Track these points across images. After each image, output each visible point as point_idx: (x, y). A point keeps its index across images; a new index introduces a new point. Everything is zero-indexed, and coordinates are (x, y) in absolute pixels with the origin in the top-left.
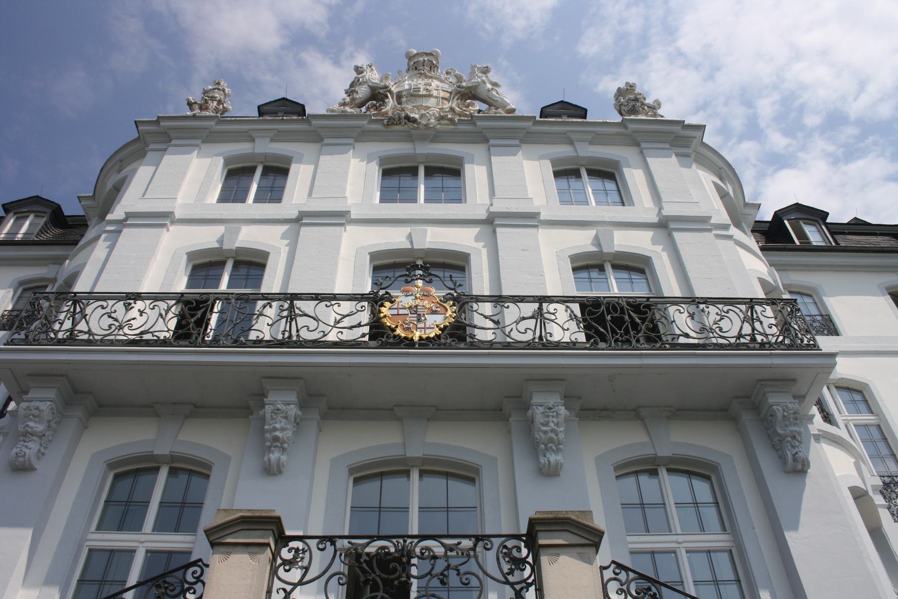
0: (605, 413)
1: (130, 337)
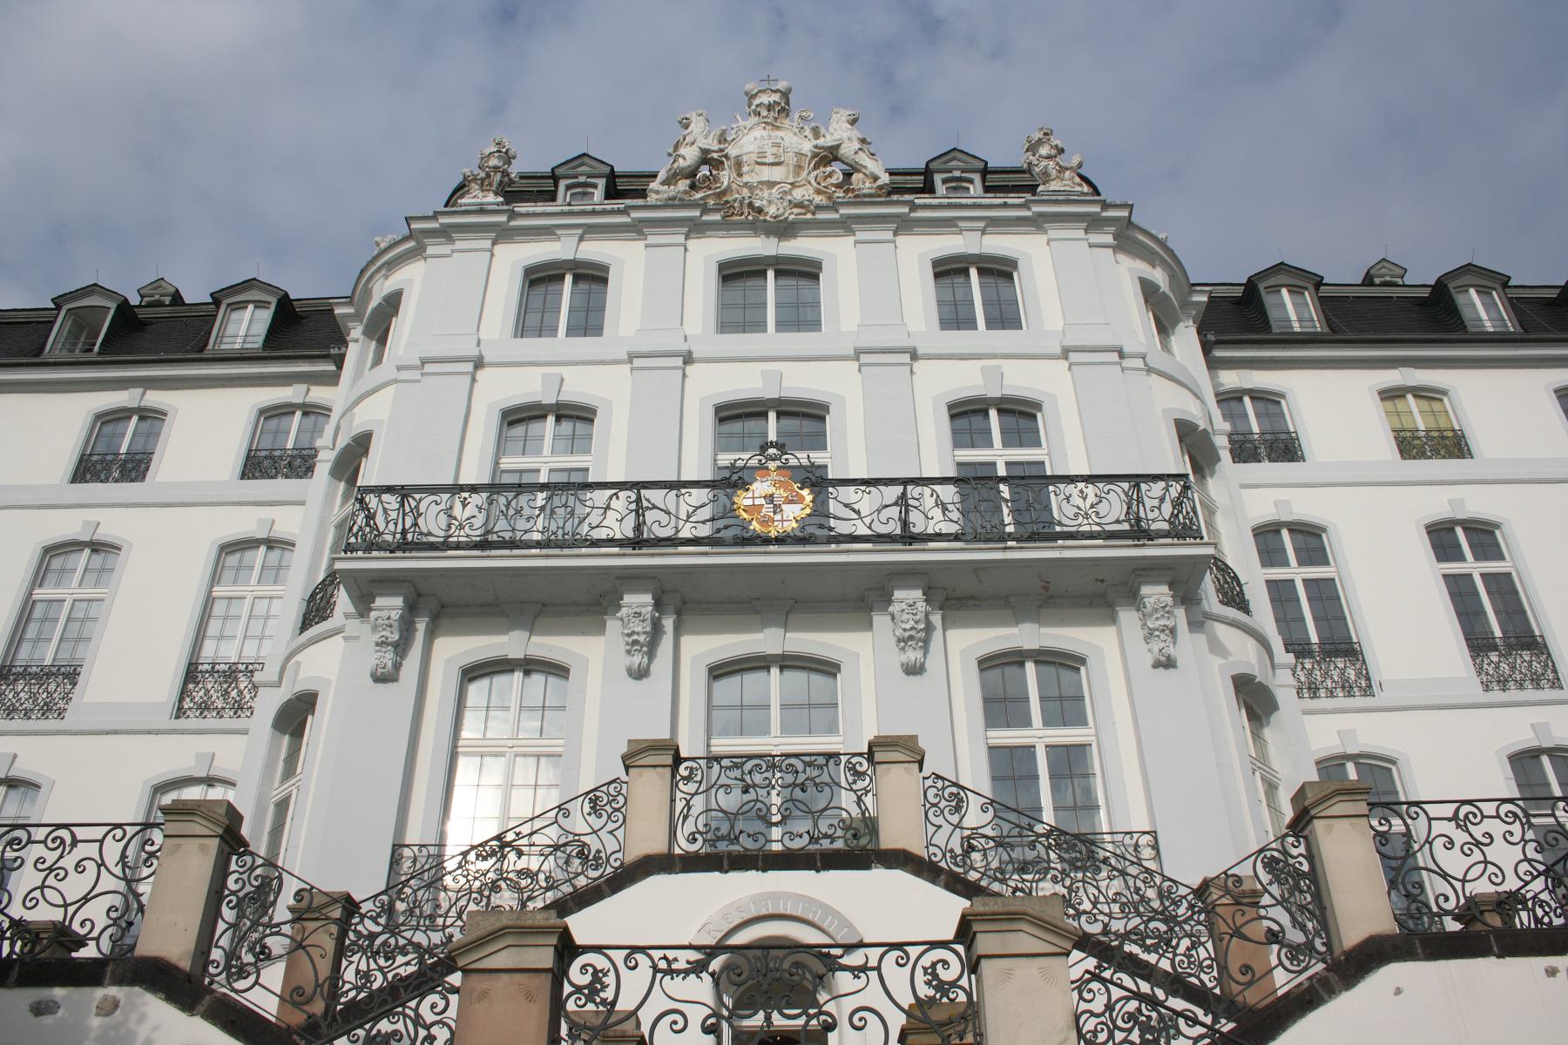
0: (972, 602)
1: (474, 539)
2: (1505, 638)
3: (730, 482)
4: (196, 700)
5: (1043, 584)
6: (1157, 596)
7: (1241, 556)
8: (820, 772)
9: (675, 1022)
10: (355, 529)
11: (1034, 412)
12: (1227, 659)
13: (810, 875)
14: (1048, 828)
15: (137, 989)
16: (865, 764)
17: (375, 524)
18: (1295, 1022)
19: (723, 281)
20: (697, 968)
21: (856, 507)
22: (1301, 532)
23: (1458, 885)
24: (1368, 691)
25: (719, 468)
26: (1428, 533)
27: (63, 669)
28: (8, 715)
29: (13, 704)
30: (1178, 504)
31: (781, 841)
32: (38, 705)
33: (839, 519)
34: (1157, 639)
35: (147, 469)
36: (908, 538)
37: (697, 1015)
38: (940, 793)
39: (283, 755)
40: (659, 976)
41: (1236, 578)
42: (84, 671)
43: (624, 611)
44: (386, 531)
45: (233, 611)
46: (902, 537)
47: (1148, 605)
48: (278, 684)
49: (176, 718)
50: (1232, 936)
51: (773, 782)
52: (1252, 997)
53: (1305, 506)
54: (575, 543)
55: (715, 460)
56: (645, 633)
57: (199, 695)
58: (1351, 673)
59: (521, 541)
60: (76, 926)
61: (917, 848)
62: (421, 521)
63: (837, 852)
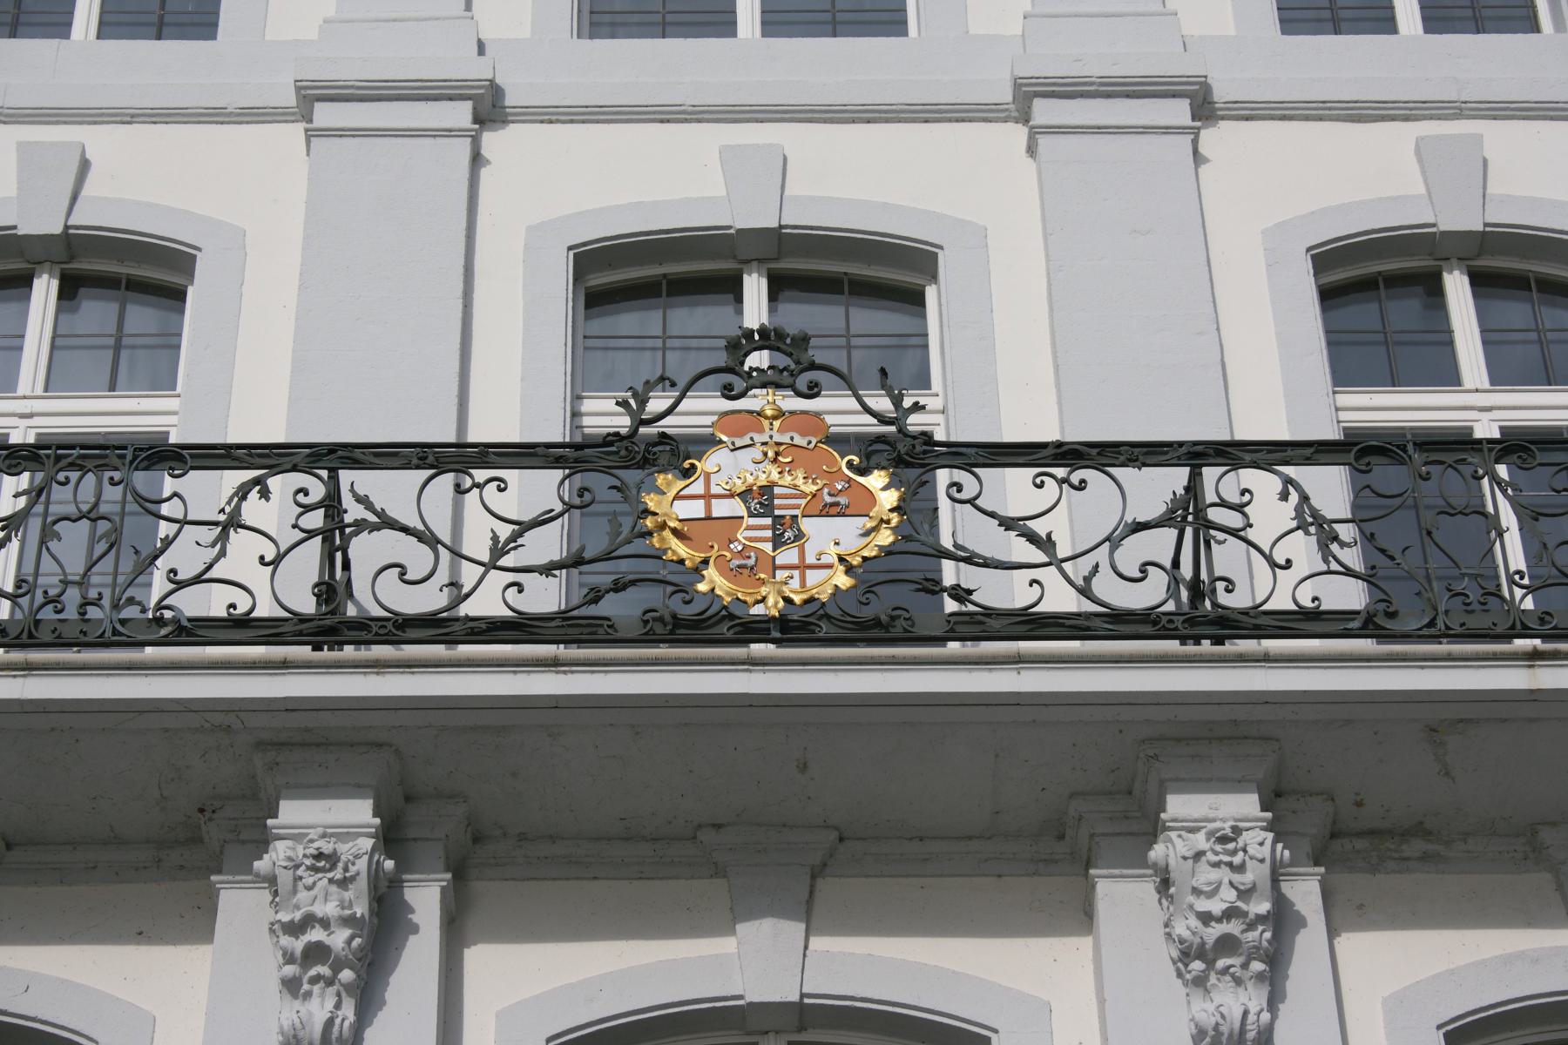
0: (1416, 847)
19: (588, 306)
21: (1040, 527)
33: (987, 563)
43: (280, 851)
55: (576, 414)
56: (348, 921)
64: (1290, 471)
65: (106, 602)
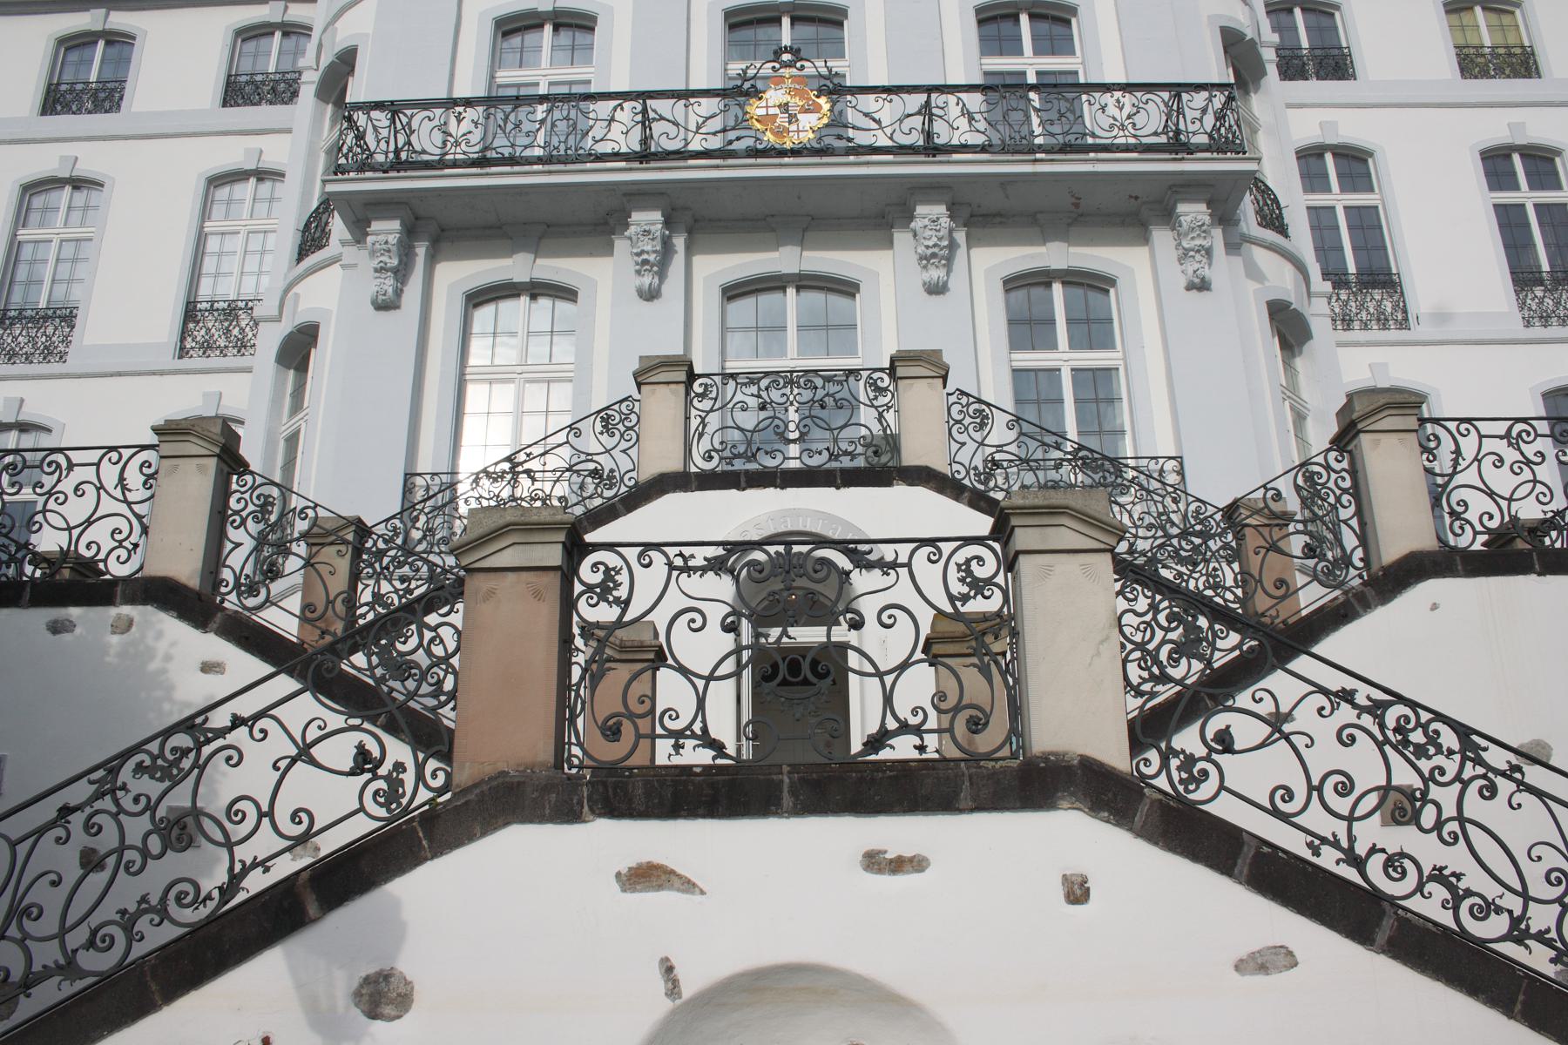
0: (998, 219)
1: (471, 156)
2: (1551, 272)
3: (739, 92)
4: (198, 339)
5: (1074, 200)
6: (1194, 215)
7: (1281, 176)
8: (839, 387)
9: (693, 621)
10: (345, 150)
11: (1068, 17)
12: (1262, 283)
13: (829, 492)
14: (1076, 446)
15: (149, 608)
16: (887, 379)
17: (365, 143)
18: (1328, 635)
20: (716, 566)
21: (876, 116)
22: (1346, 156)
23: (1504, 504)
24: (1404, 324)
25: (730, 78)
26: (1483, 159)
27: (58, 312)
28: (9, 359)
29: (12, 349)
30: (1220, 117)
31: (800, 458)
32: (38, 349)
33: (858, 129)
34: (1191, 259)
35: (121, 98)
36: (932, 149)
37: (716, 613)
38: (965, 409)
39: (289, 389)
40: (675, 573)
41: (1276, 201)
42: (80, 313)
43: (632, 230)
44: (378, 150)
45: (228, 247)
46: (925, 148)
47: (1184, 224)
48: (278, 319)
49: (179, 358)
50: (1268, 550)
51: (791, 398)
52: (1284, 612)
53: (1351, 129)
54: (578, 159)
55: (726, 70)
56: (655, 252)
57: (200, 334)
58: (1388, 306)
59: (522, 157)
60: (83, 551)
61: (941, 465)
62: (414, 139)
63: (857, 470)
64: (959, 95)
65: (573, 148)
